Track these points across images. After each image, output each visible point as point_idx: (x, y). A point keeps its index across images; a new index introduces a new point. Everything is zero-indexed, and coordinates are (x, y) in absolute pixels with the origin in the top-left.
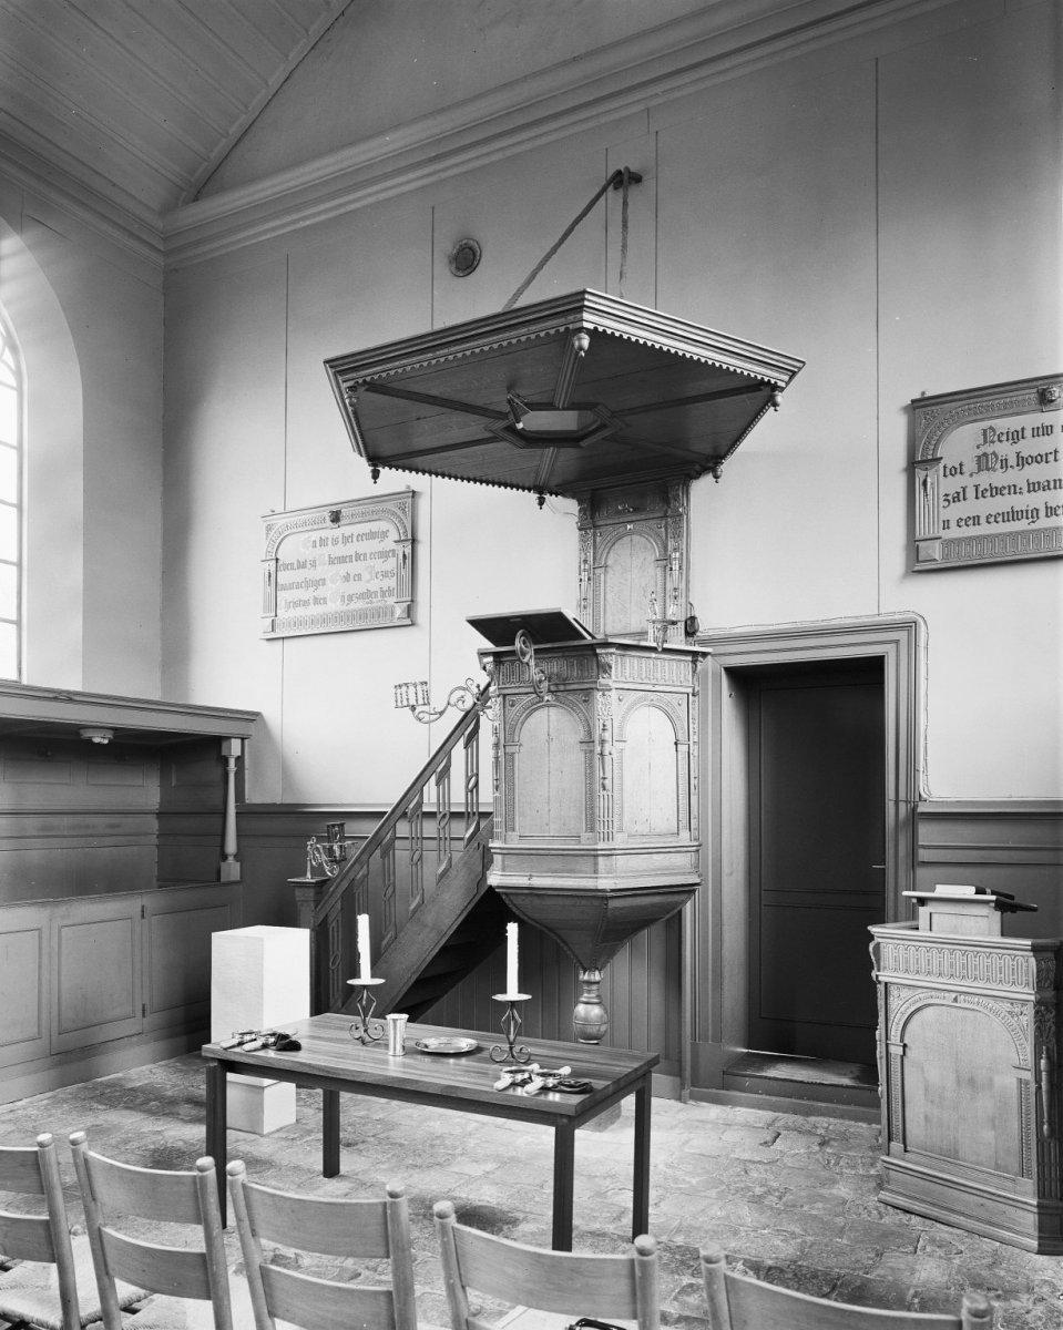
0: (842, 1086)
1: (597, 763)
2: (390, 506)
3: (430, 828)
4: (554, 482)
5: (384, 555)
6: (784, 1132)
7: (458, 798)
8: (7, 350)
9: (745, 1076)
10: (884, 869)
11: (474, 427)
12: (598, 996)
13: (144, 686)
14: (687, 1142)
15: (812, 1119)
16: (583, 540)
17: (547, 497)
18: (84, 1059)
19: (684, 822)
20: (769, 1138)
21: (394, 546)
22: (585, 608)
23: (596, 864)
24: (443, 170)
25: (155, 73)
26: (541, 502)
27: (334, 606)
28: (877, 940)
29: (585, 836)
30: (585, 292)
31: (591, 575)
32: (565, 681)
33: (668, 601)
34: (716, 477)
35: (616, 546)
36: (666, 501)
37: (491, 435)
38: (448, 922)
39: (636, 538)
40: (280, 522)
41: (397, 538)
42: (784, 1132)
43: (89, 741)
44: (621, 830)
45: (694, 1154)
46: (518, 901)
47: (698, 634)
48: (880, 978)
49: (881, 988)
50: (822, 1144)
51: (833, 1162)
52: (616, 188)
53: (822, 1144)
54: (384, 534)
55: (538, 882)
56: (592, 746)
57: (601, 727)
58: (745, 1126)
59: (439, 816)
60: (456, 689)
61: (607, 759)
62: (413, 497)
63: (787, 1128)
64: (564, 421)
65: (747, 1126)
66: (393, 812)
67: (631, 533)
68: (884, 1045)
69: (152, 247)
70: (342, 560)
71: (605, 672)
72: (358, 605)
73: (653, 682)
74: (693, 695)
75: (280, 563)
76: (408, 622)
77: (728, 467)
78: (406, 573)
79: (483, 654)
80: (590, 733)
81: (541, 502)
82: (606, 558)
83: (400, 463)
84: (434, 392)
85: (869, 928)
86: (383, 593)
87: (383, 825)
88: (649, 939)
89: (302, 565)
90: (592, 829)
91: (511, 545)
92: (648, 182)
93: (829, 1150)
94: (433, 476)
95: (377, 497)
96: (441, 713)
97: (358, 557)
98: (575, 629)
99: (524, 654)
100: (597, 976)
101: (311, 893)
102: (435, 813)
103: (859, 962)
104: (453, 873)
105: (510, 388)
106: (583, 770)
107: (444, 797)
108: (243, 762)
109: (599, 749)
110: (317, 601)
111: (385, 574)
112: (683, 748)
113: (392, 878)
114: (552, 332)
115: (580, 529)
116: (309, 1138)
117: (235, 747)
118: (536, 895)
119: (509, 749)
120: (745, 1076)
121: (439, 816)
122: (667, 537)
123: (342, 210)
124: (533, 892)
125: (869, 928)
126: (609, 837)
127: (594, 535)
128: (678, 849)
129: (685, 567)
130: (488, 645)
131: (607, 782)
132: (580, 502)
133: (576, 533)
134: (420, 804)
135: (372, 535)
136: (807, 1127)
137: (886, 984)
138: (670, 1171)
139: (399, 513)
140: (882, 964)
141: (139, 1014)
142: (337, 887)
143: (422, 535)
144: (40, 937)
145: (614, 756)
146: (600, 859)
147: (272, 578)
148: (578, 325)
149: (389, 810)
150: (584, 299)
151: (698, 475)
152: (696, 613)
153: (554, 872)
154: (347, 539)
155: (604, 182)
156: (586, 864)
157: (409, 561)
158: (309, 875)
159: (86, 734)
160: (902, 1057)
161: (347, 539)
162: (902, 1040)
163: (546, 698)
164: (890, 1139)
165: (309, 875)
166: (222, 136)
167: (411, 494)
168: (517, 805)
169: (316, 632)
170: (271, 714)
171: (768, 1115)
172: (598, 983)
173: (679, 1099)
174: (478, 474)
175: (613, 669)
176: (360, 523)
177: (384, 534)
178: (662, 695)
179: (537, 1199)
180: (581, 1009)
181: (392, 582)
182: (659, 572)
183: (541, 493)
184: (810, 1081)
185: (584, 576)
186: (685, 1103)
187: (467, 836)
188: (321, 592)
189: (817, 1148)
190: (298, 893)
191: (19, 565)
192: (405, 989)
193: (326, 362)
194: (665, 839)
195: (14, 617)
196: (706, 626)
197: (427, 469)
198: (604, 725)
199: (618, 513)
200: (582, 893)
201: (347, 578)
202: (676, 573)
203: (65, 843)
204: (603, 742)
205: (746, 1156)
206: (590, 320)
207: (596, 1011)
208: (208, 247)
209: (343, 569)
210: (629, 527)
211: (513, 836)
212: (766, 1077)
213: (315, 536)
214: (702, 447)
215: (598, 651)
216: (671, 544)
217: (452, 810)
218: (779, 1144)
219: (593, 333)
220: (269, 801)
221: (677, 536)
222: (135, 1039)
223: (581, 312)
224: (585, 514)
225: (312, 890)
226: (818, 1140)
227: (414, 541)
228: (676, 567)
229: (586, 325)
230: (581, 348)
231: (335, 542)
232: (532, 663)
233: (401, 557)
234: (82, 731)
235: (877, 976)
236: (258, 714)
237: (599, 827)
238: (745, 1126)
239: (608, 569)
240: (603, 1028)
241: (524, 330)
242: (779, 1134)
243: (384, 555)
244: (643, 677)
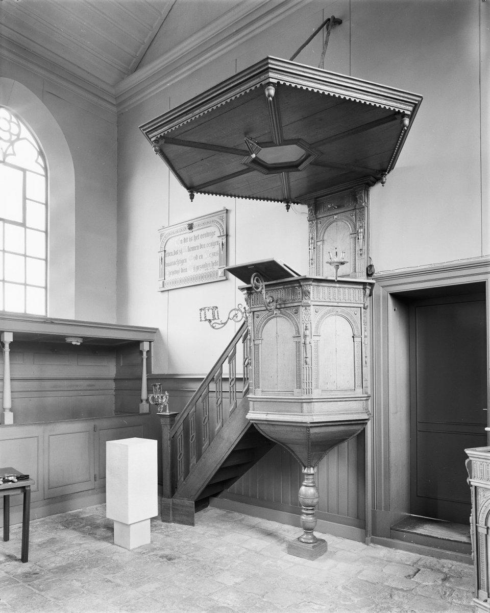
0: (461, 542)
1: (302, 349)
2: (216, 218)
3: (226, 387)
4: (293, 196)
5: (213, 244)
6: (422, 569)
7: (240, 372)
8: (40, 157)
9: (403, 531)
10: (486, 411)
12: (313, 482)
13: (110, 319)
14: (360, 572)
15: (443, 561)
16: (311, 227)
17: (195, 194)
18: (62, 501)
19: (359, 382)
20: (411, 573)
21: (218, 239)
22: (312, 264)
23: (302, 407)
24: (241, 38)
25: (103, 13)
26: (288, 208)
27: (191, 273)
28: (471, 458)
29: (296, 391)
30: (268, 58)
31: (315, 246)
32: (284, 302)
33: (357, 257)
34: (383, 183)
35: (328, 229)
36: (355, 200)
37: (245, 167)
39: (339, 223)
40: (166, 232)
41: (219, 235)
42: (422, 569)
43: (70, 344)
44: (317, 387)
45: (363, 580)
46: (262, 427)
47: (375, 275)
48: (472, 483)
49: (473, 489)
50: (444, 580)
51: (448, 593)
53: (444, 580)
54: (213, 233)
55: (271, 417)
56: (300, 341)
57: (304, 328)
58: (399, 563)
59: (230, 380)
60: (232, 311)
61: (308, 346)
62: (227, 213)
63: (424, 566)
64: (291, 153)
65: (400, 563)
66: (207, 377)
67: (336, 220)
68: (475, 527)
69: (112, 104)
70: (194, 249)
71: (306, 295)
72: (202, 271)
73: (337, 301)
74: (364, 308)
75: (166, 252)
76: (225, 278)
77: (389, 178)
78: (223, 253)
79: (242, 289)
80: (298, 332)
81: (288, 208)
82: (323, 235)
83: (210, 188)
86: (213, 264)
87: (202, 385)
88: (347, 447)
89: (176, 253)
90: (300, 388)
91: (274, 230)
92: (346, 24)
93: (447, 584)
94: (237, 198)
95: (215, 213)
96: (225, 324)
97: (201, 246)
99: (257, 288)
100: (312, 471)
101: (168, 420)
102: (228, 378)
103: (462, 470)
104: (237, 410)
106: (295, 353)
107: (233, 370)
108: (151, 353)
109: (303, 340)
110: (183, 271)
111: (214, 254)
112: (357, 340)
113: (208, 413)
114: (253, 88)
115: (309, 221)
116: (152, 553)
117: (145, 347)
118: (273, 425)
119: (256, 342)
120: (403, 531)
121: (230, 380)
122: (356, 220)
123: (194, 70)
126: (309, 392)
127: (317, 223)
128: (355, 399)
129: (366, 237)
130: (244, 285)
131: (308, 360)
133: (307, 224)
134: (221, 373)
135: (207, 235)
136: (438, 566)
137: (476, 487)
138: (343, 592)
139: (220, 222)
140: (473, 474)
141: (92, 478)
142: (180, 418)
143: (231, 232)
144: (38, 441)
145: (313, 345)
146: (304, 404)
147: (163, 260)
148: (267, 81)
149: (205, 377)
150: (268, 63)
151: (374, 183)
152: (373, 263)
153: (279, 412)
154: (196, 238)
155: (322, 23)
156: (296, 407)
157: (225, 246)
158: (168, 411)
159: (68, 340)
160: (486, 535)
161: (196, 238)
162: (486, 524)
163: (275, 312)
164: (479, 588)
165: (168, 411)
166: (142, 44)
167: (225, 211)
168: (260, 373)
169: (186, 286)
170: (163, 329)
171: (414, 556)
172: (313, 474)
173: (364, 542)
174: (250, 194)
176: (202, 229)
177: (213, 233)
178: (344, 308)
179: (257, 605)
180: (303, 489)
181: (217, 258)
182: (352, 240)
183: (288, 202)
184: (442, 537)
185: (312, 246)
186: (368, 545)
187: (244, 391)
188: (185, 266)
189: (440, 582)
190: (162, 420)
191: (46, 260)
192: (214, 473)
194: (346, 393)
195: (44, 285)
196: (378, 270)
198: (306, 327)
199: (329, 209)
200: (298, 424)
201: (196, 258)
202: (361, 241)
203: (66, 393)
204: (305, 336)
205: (394, 585)
206: (274, 77)
207: (312, 491)
208: (134, 100)
209: (194, 253)
210: (335, 217)
211: (259, 391)
212: (415, 533)
213: (182, 238)
214: (374, 164)
215: (302, 284)
216: (358, 224)
217: (237, 377)
218: (417, 578)
219: (278, 86)
220: (163, 373)
221: (362, 219)
222: (90, 492)
223: (268, 72)
224: (312, 212)
225: (168, 419)
226: (442, 576)
227: (227, 235)
228: (361, 237)
229: (271, 80)
230: (269, 96)
231: (191, 239)
232: (264, 291)
233: (221, 245)
234: (66, 339)
235: (470, 482)
236: (157, 329)
237: (304, 386)
238: (399, 563)
239: (325, 242)
240: (315, 501)
241: (238, 90)
242: (419, 570)
243: (213, 244)
244: (347, 299)
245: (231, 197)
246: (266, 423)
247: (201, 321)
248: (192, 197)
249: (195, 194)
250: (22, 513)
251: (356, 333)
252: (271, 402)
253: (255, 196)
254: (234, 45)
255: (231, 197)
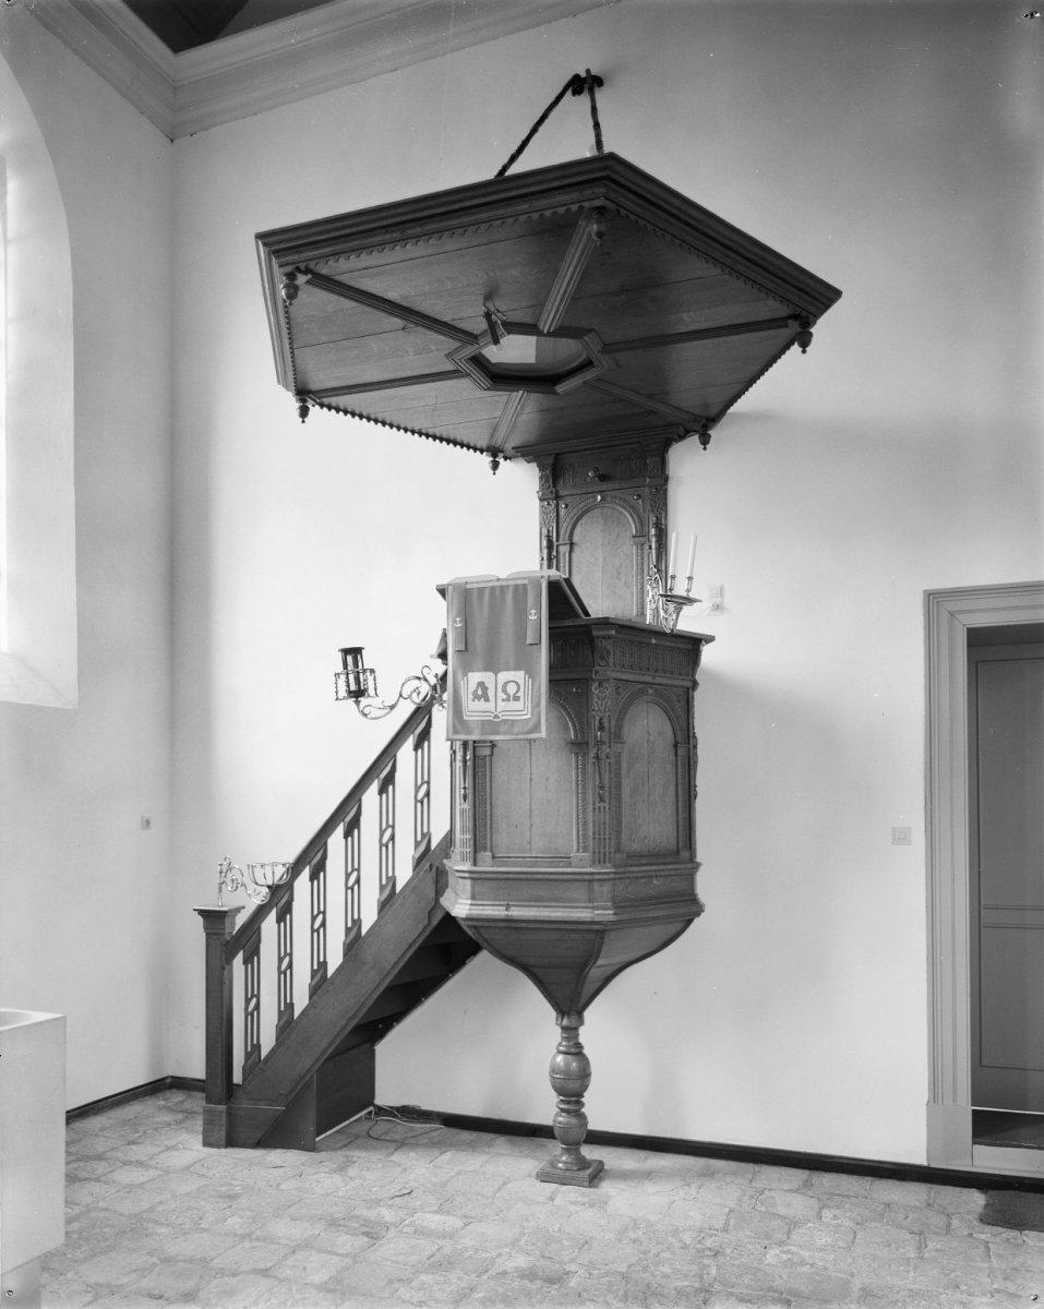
11: (432, 351)
17: (501, 461)
26: (495, 466)
38: (392, 958)
52: (574, 94)
55: (517, 912)
71: (602, 658)
81: (495, 466)
84: (392, 295)
85: (242, 952)
96: (392, 707)
98: (572, 607)
105: (488, 297)
115: (541, 500)
124: (509, 924)
125: (242, 952)
132: (541, 467)
153: (537, 901)
175: (612, 655)
183: (494, 455)
193: (260, 236)
197: (365, 414)
224: (547, 481)
245: (455, 446)
246: (503, 924)
247: (337, 699)
248: (304, 412)
249: (501, 461)
250: (919, 1158)
251: (679, 739)
252: (556, 880)
253: (431, 432)
254: (751, 248)
255: (455, 446)
